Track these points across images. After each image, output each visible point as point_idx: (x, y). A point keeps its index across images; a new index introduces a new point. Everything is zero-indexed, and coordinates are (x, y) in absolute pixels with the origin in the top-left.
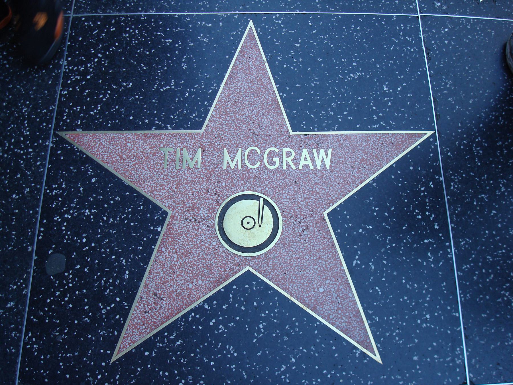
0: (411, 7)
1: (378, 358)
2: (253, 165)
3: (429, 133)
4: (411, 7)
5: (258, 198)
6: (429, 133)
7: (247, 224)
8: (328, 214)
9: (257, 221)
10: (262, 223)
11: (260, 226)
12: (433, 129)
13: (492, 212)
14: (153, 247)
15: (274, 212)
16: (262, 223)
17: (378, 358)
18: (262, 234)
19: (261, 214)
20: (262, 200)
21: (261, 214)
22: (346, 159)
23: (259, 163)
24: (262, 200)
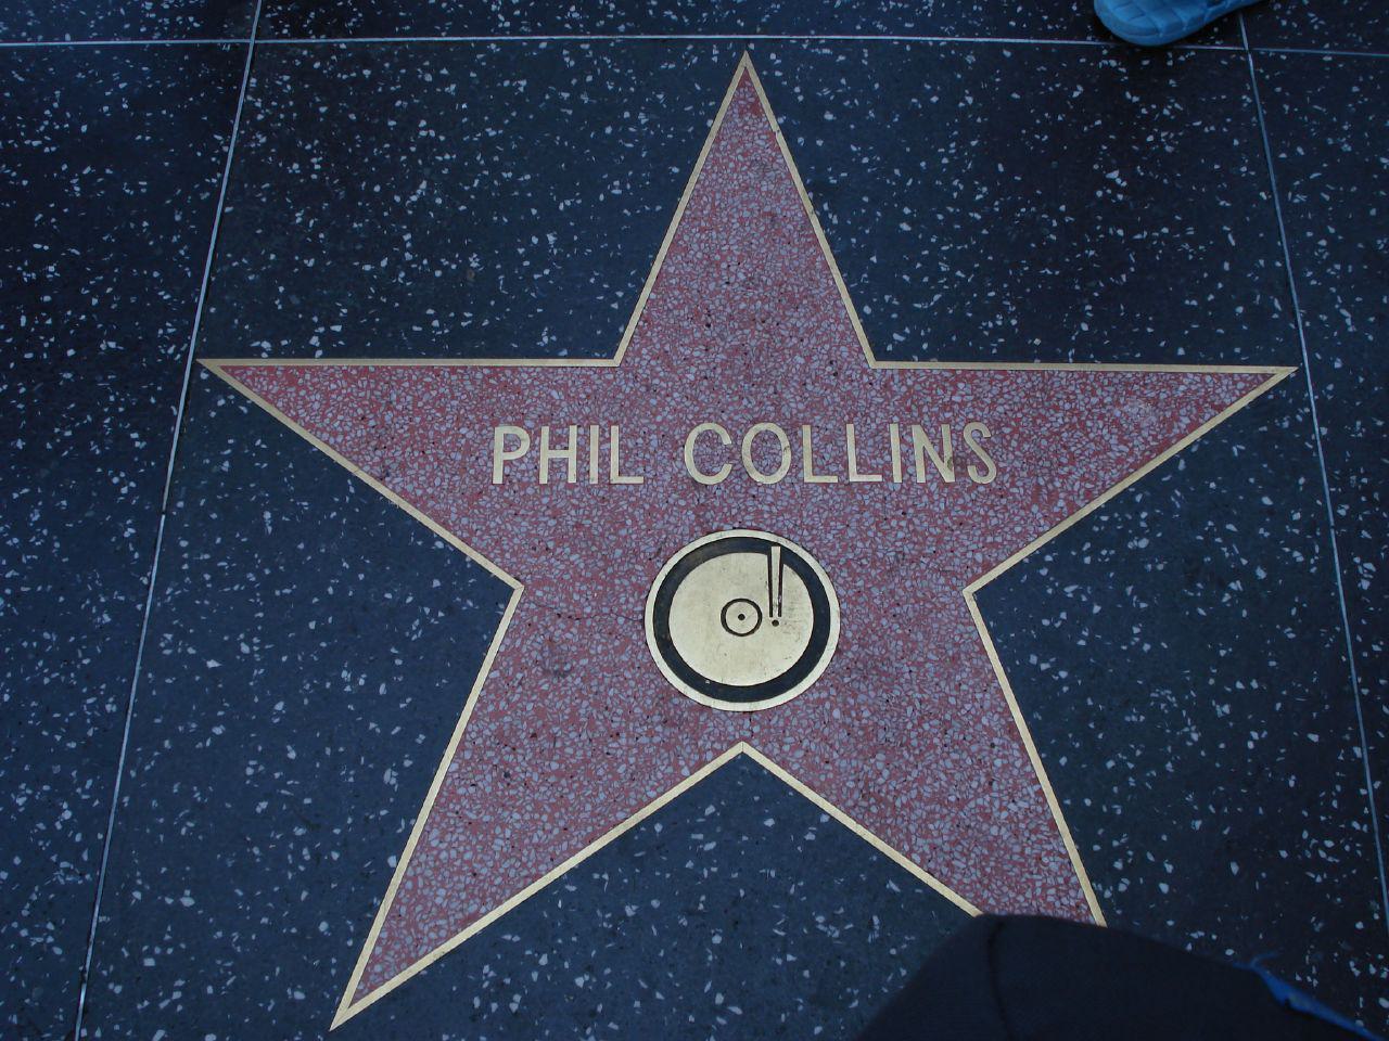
0: (464, 324)
1: (344, 1013)
2: (709, 473)
3: (1281, 373)
4: (464, 324)
5: (763, 547)
6: (1281, 373)
7: (735, 629)
8: (511, 590)
9: (765, 610)
10: (780, 615)
11: (775, 623)
12: (1297, 361)
13: (1347, 511)
14: (824, 819)
15: (676, 576)
16: (780, 615)
17: (344, 1013)
18: (780, 650)
19: (776, 608)
20: (776, 551)
21: (773, 586)
22: (493, 452)
23: (727, 468)
24: (776, 551)
